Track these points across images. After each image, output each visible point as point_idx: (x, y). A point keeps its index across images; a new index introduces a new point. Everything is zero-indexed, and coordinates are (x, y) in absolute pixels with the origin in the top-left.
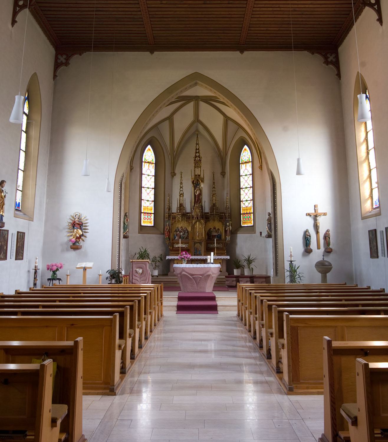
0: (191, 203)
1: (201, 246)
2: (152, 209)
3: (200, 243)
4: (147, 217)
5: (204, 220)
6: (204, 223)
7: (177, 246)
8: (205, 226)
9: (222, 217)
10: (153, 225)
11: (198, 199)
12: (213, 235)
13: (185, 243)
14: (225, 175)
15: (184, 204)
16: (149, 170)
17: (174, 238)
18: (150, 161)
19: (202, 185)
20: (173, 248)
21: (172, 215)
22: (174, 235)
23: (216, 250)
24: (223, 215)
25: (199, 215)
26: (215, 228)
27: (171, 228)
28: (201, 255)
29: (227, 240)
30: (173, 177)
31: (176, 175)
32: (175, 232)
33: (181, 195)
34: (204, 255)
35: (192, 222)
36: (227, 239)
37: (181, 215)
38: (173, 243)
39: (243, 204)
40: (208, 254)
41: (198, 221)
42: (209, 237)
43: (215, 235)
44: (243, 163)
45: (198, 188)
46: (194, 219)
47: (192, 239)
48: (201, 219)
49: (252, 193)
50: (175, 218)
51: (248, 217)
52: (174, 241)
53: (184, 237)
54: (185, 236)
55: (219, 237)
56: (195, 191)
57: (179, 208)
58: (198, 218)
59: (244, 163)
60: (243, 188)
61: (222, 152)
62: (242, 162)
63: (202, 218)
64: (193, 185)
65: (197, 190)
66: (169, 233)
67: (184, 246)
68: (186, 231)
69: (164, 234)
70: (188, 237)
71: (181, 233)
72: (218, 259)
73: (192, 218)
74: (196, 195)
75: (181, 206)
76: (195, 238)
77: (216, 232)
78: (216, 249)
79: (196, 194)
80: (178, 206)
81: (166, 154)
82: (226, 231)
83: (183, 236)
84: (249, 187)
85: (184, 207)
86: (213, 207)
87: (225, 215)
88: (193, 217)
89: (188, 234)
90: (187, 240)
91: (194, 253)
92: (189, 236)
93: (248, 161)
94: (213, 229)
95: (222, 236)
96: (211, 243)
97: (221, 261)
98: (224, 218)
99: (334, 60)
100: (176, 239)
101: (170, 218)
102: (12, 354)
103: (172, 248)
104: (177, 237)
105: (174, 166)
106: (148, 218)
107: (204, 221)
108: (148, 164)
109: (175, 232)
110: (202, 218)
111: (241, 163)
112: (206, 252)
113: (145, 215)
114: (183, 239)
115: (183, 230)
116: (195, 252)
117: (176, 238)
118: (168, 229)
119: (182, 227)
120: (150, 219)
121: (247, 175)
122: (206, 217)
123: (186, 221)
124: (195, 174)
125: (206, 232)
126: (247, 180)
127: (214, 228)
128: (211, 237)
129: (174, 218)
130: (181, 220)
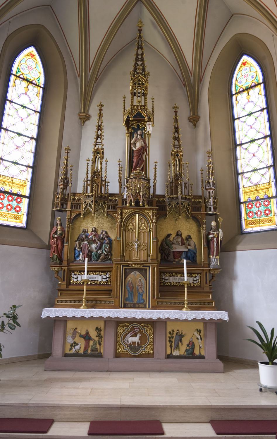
0: (121, 171)
1: (143, 280)
2: (24, 186)
3: (143, 271)
4: (12, 203)
5: (153, 209)
7: (79, 277)
8: (156, 227)
9: (196, 209)
10: (22, 222)
11: (137, 160)
12: (174, 252)
13: (103, 272)
14: (198, 120)
15: (104, 172)
16: (26, 96)
17: (75, 258)
18: (30, 77)
19: (149, 128)
20: (67, 287)
22: (75, 249)
23: (188, 292)
24: (201, 200)
26: (179, 234)
28: (145, 307)
29: (211, 266)
30: (84, 123)
31: (91, 119)
32: (77, 243)
33: (98, 153)
34: (154, 308)
35: (121, 214)
36: (212, 264)
37: (93, 199)
38: (70, 271)
39: (245, 181)
40: (164, 305)
41: (136, 213)
42: (166, 256)
43: (181, 253)
44: (239, 92)
45: (139, 137)
46: (128, 205)
47: (121, 260)
48: (146, 206)
49: (269, 148)
51: (262, 208)
52: (72, 265)
53: (99, 257)
54: (102, 253)
55: (192, 257)
56: (132, 141)
57: (89, 183)
58: (137, 203)
59: (243, 91)
60: (244, 144)
61: (192, 75)
62: (236, 90)
63: (148, 204)
64: (126, 132)
65: (135, 141)
66: (59, 243)
67: (98, 278)
68: (103, 239)
69: (48, 247)
70: (111, 255)
71: (93, 246)
72: (194, 320)
73: (123, 204)
74: (133, 150)
75: (96, 178)
77: (183, 244)
78: (186, 289)
79: (134, 149)
80: (87, 177)
81: (69, 72)
82: (208, 242)
83: (97, 252)
84: (261, 138)
85: (103, 179)
86: (174, 184)
87: (205, 202)
89: (111, 247)
90: (106, 262)
91: (126, 299)
92: (113, 253)
93: (253, 84)
94: (174, 235)
97: (201, 327)
98: (203, 209)
100: (78, 259)
101: (67, 204)
103: (65, 283)
104: (81, 254)
105: (86, 98)
106: (9, 205)
107: (155, 212)
108: (25, 83)
109: (77, 243)
110: (150, 203)
111: (234, 92)
112: (158, 298)
113: (10, 198)
114: (97, 260)
115: (99, 237)
116: (127, 297)
117: (79, 256)
119: (95, 230)
120: (18, 209)
121: (252, 113)
122: (160, 207)
124: (132, 102)
125: (158, 241)
126: (254, 124)
128: (171, 257)
129: (76, 205)
130: (93, 211)
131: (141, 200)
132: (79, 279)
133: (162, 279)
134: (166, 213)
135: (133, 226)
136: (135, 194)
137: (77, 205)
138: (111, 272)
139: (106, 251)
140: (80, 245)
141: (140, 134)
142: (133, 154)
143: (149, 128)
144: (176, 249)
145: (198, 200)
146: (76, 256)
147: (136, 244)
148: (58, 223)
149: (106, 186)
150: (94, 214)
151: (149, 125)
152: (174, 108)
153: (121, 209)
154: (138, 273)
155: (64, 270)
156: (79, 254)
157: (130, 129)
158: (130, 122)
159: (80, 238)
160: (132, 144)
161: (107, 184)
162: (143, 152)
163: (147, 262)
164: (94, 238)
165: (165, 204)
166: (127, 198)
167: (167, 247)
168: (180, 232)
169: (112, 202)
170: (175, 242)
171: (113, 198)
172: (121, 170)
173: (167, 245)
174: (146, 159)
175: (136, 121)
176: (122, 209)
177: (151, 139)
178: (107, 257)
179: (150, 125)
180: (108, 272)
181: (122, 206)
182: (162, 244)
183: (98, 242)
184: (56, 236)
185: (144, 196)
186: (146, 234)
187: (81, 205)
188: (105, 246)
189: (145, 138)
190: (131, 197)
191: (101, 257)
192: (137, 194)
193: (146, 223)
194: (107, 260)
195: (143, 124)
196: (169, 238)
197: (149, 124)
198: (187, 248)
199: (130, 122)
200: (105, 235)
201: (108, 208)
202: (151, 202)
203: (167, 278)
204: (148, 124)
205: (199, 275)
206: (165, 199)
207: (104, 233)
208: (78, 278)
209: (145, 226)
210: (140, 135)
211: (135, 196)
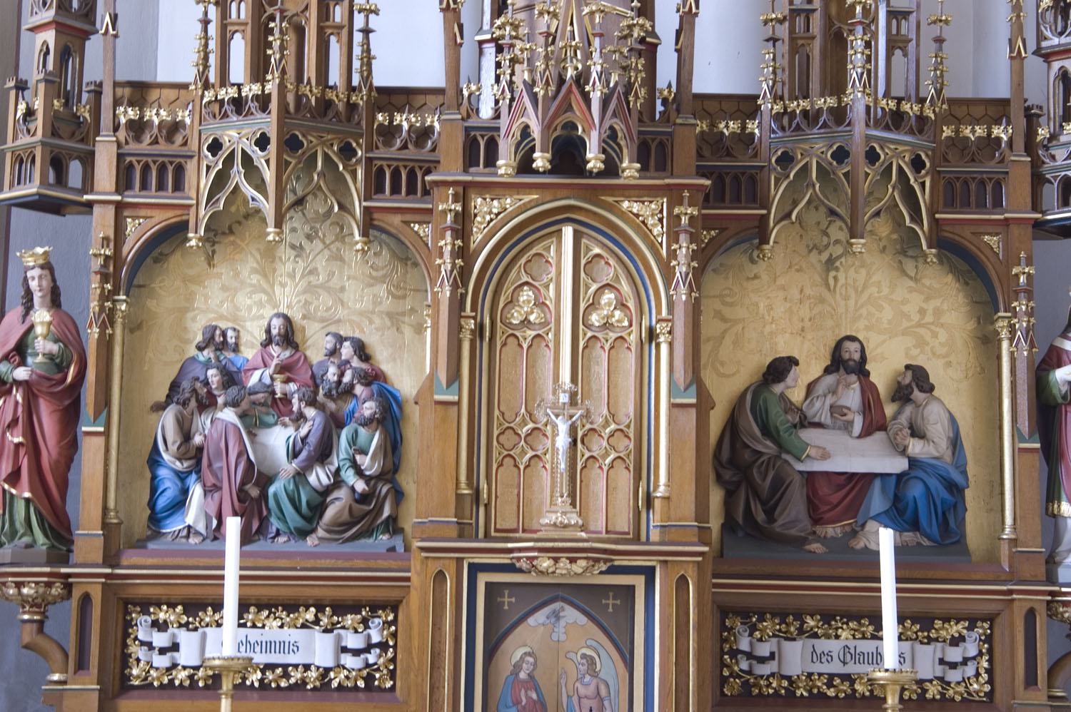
1: (609, 664)
3: (607, 606)
5: (674, 194)
6: (684, 249)
12: (810, 477)
13: (341, 608)
17: (155, 520)
21: (128, 114)
22: (154, 460)
25: (596, 97)
26: (846, 362)
27: (92, 334)
32: (168, 418)
37: (268, 123)
38: (125, 605)
43: (859, 483)
48: (630, 169)
50: (171, 174)
52: (134, 564)
53: (318, 508)
54: (338, 482)
55: (931, 509)
63: (643, 156)
68: (346, 393)
71: (278, 439)
73: (470, 160)
76: (505, 519)
77: (874, 424)
83: (300, 476)
87: (1030, 145)
88: (479, 146)
90: (366, 544)
92: (408, 481)
94: (811, 367)
95: (970, 496)
96: (782, 615)
99: (929, 696)
100: (173, 526)
101: (88, 160)
102: (688, 19)
104: (196, 492)
107: (687, 212)
110: (654, 154)
114: (303, 534)
115: (315, 382)
117: (180, 504)
118: (43, 345)
119: (289, 337)
123: (369, 225)
125: (704, 404)
127: (837, 363)
129: (152, 169)
130: (268, 207)
132: (187, 656)
133: (734, 653)
134: (764, 218)
135: (540, 304)
137: (162, 169)
138: (394, 607)
139: (359, 472)
140: (186, 436)
144: (825, 456)
145: (980, 131)
146: (162, 502)
147: (563, 427)
148: (34, 285)
149: (358, 37)
150: (279, 224)
153: (460, 190)
154: (571, 615)
155: (86, 599)
156: (185, 492)
159: (186, 384)
161: (359, 21)
163: (637, 539)
164: (279, 388)
166: (497, 116)
167: (767, 447)
168: (852, 347)
169: (398, 143)
170: (819, 409)
171: (403, 120)
173: (767, 431)
176: (464, 192)
178: (373, 513)
180: (375, 607)
181: (466, 171)
182: (732, 424)
183: (310, 412)
184: (21, 374)
186: (630, 360)
187: (191, 167)
188: (353, 440)
191: (330, 513)
193: (625, 287)
194: (368, 532)
196: (778, 388)
198: (903, 452)
200: (356, 363)
201: (375, 185)
202: (662, 145)
203: (764, 650)
205: (982, 629)
206: (753, 126)
207: (347, 350)
208: (175, 647)
209: (622, 305)
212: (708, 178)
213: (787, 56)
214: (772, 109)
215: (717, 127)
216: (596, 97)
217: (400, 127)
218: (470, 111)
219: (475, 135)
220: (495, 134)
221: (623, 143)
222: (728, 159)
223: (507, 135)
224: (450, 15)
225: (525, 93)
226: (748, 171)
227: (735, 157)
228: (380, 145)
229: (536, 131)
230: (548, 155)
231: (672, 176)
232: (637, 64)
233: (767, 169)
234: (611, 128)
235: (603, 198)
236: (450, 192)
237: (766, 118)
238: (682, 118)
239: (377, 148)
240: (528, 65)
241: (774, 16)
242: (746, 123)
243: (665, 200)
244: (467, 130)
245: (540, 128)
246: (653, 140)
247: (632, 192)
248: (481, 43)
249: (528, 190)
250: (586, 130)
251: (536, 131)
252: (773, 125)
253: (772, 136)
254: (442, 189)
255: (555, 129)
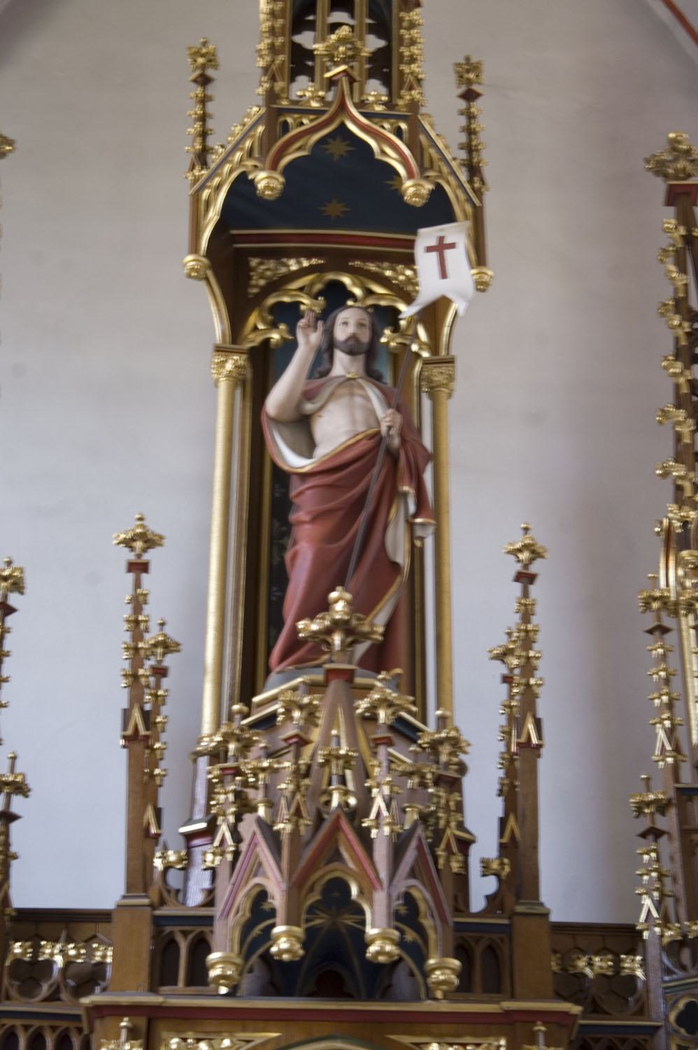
25: (381, 835)
56: (276, 399)
64: (218, 327)
73: (162, 974)
74: (282, 477)
79: (294, 461)
131: (380, 897)
136: (307, 821)
141: (354, 337)
142: (283, 548)
143: (444, 275)
151: (441, 247)
152: (517, 612)
153: (142, 1022)
157: (253, 319)
158: (254, 262)
160: (275, 421)
162: (390, 493)
165: (641, 1011)
166: (210, 902)
169: (45, 989)
171: (56, 954)
172: (160, 672)
174: (416, 555)
175: (309, 257)
177: (453, 408)
179: (448, 253)
181: (153, 989)
185: (410, 856)
189: (401, 361)
190: (258, 869)
192: (320, 848)
195: (384, 282)
197: (441, 239)
199: (254, 262)
202: (491, 949)
204: (433, 242)
206: (633, 965)
210: (351, 353)
211: (308, 854)
212: (577, 1003)
213: (678, 857)
214: (662, 936)
215: (575, 967)
216: (381, 835)
217: (49, 963)
218: (165, 894)
219: (172, 933)
220: (206, 929)
221: (427, 922)
222: (594, 1015)
223: (226, 914)
224: (138, 747)
225: (259, 838)
226: (632, 1037)
227: (607, 1013)
228: (13, 993)
229: (277, 899)
230: (299, 931)
231: (513, 997)
232: (448, 801)
233: (662, 1033)
234: (408, 899)
235: (393, 1037)
236: (123, 1024)
237: (653, 951)
238: (523, 904)
239: (8, 998)
240: (266, 795)
241: (652, 797)
242: (621, 961)
243: (503, 1042)
244: (158, 922)
245: (284, 886)
246: (478, 941)
247: (446, 1028)
248: (190, 837)
249: (261, 1024)
250: (366, 891)
251: (277, 899)
252: (666, 961)
253: (667, 978)
254: (109, 1021)
255: (312, 889)
